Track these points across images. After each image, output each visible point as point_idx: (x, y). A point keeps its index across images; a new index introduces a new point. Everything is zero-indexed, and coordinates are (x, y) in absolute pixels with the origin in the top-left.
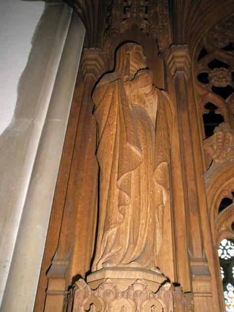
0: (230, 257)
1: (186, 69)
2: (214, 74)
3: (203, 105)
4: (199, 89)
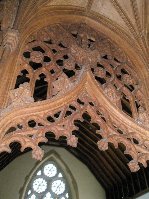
0: (44, 180)
1: (13, 45)
2: (33, 54)
3: (20, 70)
4: (20, 59)
